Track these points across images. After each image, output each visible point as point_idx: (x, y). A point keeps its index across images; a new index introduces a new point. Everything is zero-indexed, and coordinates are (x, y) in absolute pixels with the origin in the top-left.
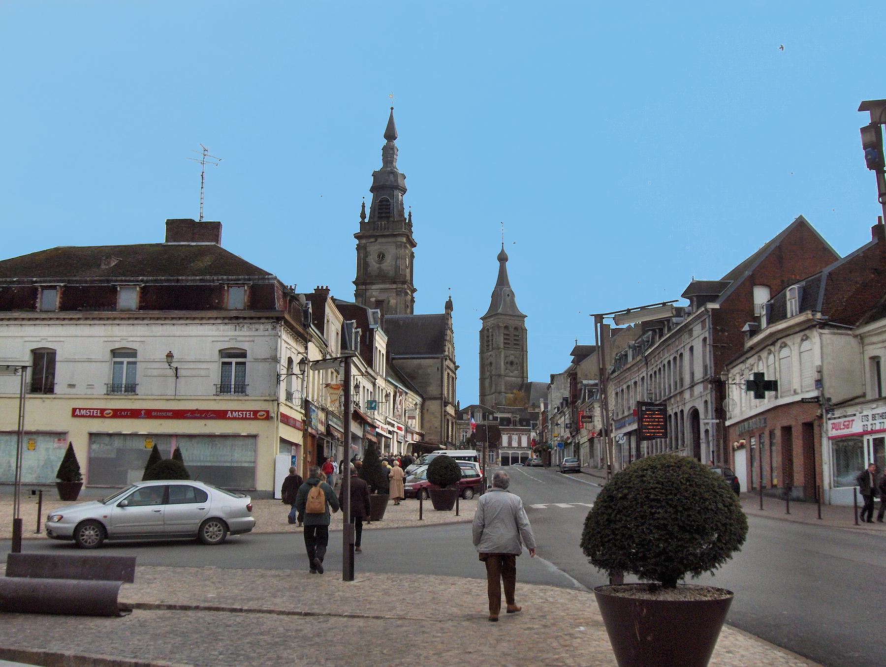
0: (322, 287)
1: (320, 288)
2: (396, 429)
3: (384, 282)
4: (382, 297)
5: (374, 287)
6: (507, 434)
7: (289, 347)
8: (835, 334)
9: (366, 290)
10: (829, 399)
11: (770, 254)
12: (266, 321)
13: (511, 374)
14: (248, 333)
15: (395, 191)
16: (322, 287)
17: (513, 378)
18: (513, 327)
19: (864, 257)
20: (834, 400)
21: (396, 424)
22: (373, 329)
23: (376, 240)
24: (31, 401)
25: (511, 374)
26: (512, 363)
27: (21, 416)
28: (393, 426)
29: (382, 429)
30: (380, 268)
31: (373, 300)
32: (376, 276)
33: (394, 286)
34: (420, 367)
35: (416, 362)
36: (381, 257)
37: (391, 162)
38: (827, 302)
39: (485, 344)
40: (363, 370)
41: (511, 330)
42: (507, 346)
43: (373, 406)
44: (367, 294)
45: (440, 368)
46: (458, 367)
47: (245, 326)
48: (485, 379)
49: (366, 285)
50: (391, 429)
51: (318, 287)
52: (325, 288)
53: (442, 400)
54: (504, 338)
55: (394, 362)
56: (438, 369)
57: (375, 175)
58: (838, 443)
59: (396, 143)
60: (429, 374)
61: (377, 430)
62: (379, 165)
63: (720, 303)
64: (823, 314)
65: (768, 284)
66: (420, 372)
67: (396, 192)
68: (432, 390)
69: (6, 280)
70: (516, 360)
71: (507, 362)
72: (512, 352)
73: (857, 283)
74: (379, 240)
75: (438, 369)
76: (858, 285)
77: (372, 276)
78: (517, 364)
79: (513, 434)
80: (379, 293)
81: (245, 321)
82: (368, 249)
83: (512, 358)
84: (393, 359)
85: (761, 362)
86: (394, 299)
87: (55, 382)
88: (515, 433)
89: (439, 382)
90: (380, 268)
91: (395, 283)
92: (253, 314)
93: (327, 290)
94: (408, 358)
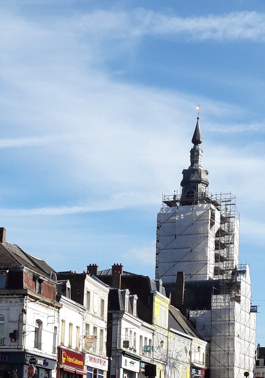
0: (93, 264)
1: (116, 265)
7: (37, 313)
12: (17, 296)
14: (5, 305)
15: (199, 184)
16: (117, 264)
24: (114, 355)
27: (106, 371)
37: (197, 162)
43: (148, 349)
47: (4, 300)
51: (115, 264)
52: (119, 265)
57: (185, 172)
59: (200, 146)
62: (187, 165)
67: (200, 186)
81: (4, 297)
87: (42, 343)
92: (7, 291)
93: (121, 266)
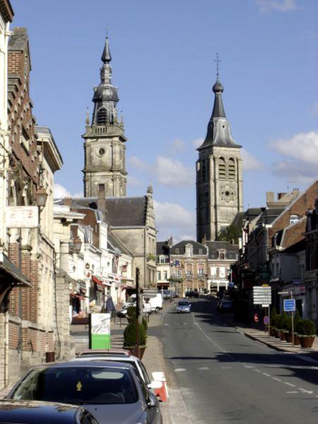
2: (114, 280)
3: (104, 171)
5: (97, 174)
13: (227, 204)
20: (285, 282)
21: (114, 277)
25: (227, 204)
26: (227, 193)
28: (112, 278)
29: (106, 282)
30: (100, 160)
31: (96, 183)
32: (98, 166)
33: (111, 173)
34: (130, 235)
35: (127, 231)
38: (285, 241)
39: (206, 170)
40: (95, 251)
41: (227, 160)
42: (223, 176)
44: (92, 179)
48: (203, 208)
50: (111, 280)
53: (145, 256)
60: (136, 240)
66: (130, 238)
70: (231, 191)
71: (223, 193)
72: (228, 183)
74: (99, 140)
82: (92, 147)
83: (227, 188)
89: (143, 245)
90: (100, 160)
91: (112, 171)
94: (109, 354)
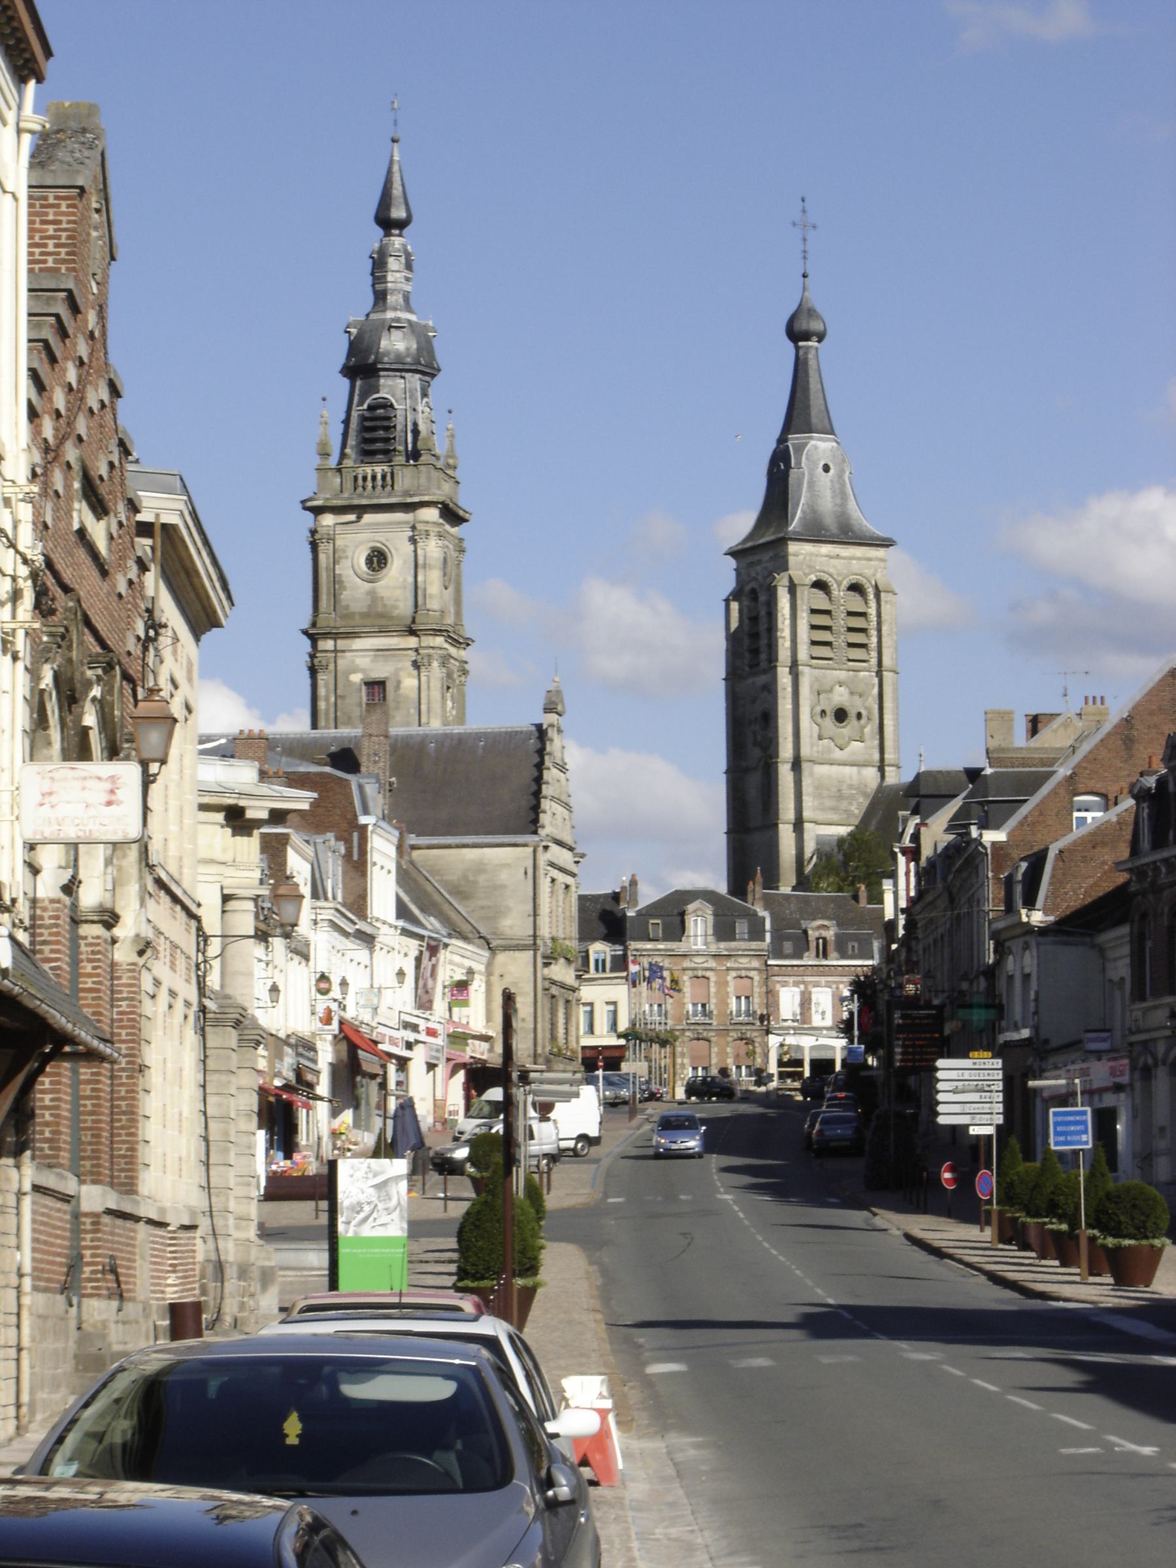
3: (383, 631)
4: (379, 671)
5: (358, 644)
6: (796, 984)
8: (1065, 944)
9: (335, 651)
10: (1046, 1041)
11: (1109, 734)
13: (838, 754)
17: (847, 770)
18: (845, 583)
19: (1119, 823)
20: (1054, 1043)
21: (423, 1025)
22: (366, 826)
23: (359, 518)
25: (838, 754)
26: (841, 715)
29: (393, 1041)
30: (372, 594)
31: (356, 678)
32: (365, 615)
33: (412, 642)
36: (378, 559)
40: (350, 929)
45: (530, 871)
46: (583, 856)
49: (335, 640)
54: (814, 627)
55: (416, 854)
56: (526, 873)
58: (372, 1206)
61: (380, 1046)
63: (1008, 830)
64: (1046, 914)
65: (1103, 791)
66: (482, 879)
68: (511, 927)
69: (111, 1055)
71: (823, 712)
72: (842, 675)
73: (1104, 863)
74: (368, 518)
75: (526, 873)
76: (1106, 867)
77: (354, 613)
78: (859, 716)
79: (817, 985)
80: (372, 661)
83: (840, 697)
84: (413, 847)
85: (1027, 952)
86: (410, 676)
88: (823, 980)
90: (372, 594)
